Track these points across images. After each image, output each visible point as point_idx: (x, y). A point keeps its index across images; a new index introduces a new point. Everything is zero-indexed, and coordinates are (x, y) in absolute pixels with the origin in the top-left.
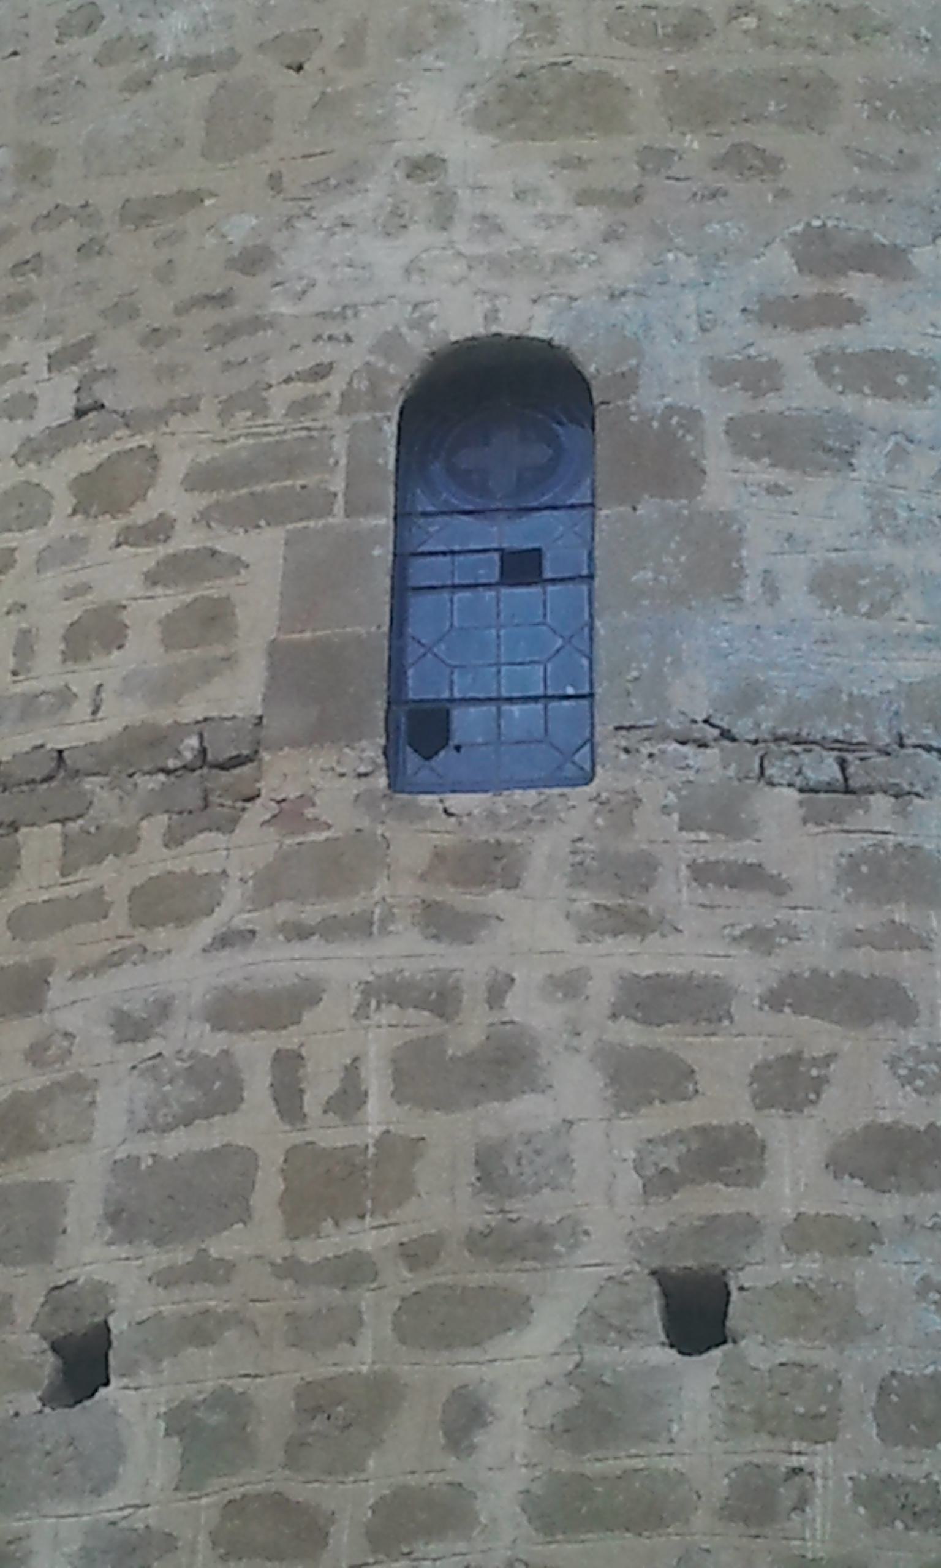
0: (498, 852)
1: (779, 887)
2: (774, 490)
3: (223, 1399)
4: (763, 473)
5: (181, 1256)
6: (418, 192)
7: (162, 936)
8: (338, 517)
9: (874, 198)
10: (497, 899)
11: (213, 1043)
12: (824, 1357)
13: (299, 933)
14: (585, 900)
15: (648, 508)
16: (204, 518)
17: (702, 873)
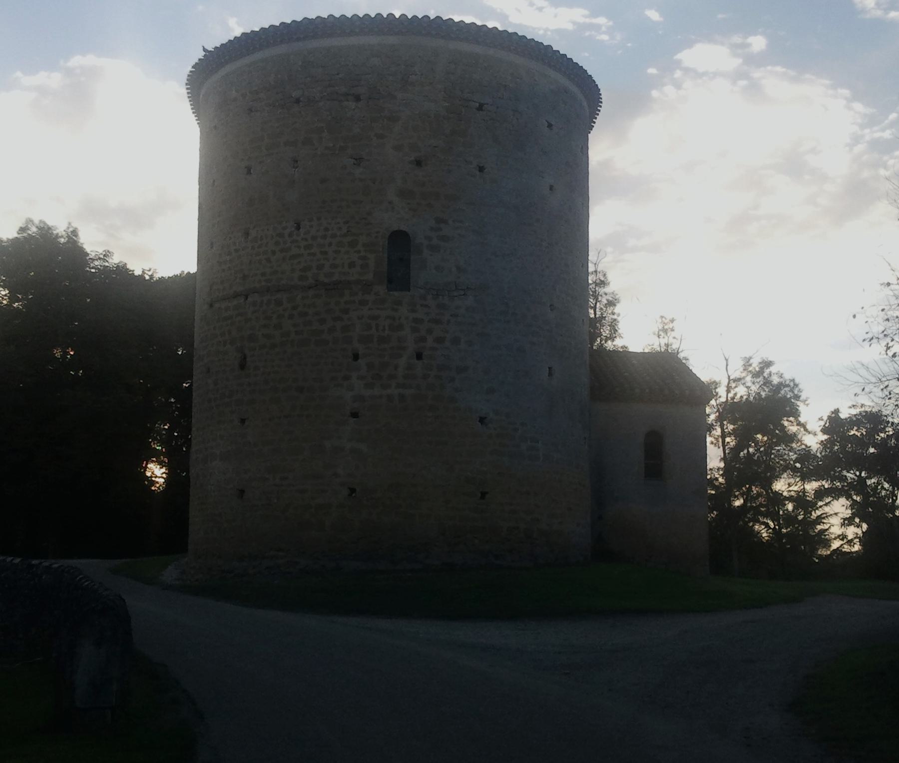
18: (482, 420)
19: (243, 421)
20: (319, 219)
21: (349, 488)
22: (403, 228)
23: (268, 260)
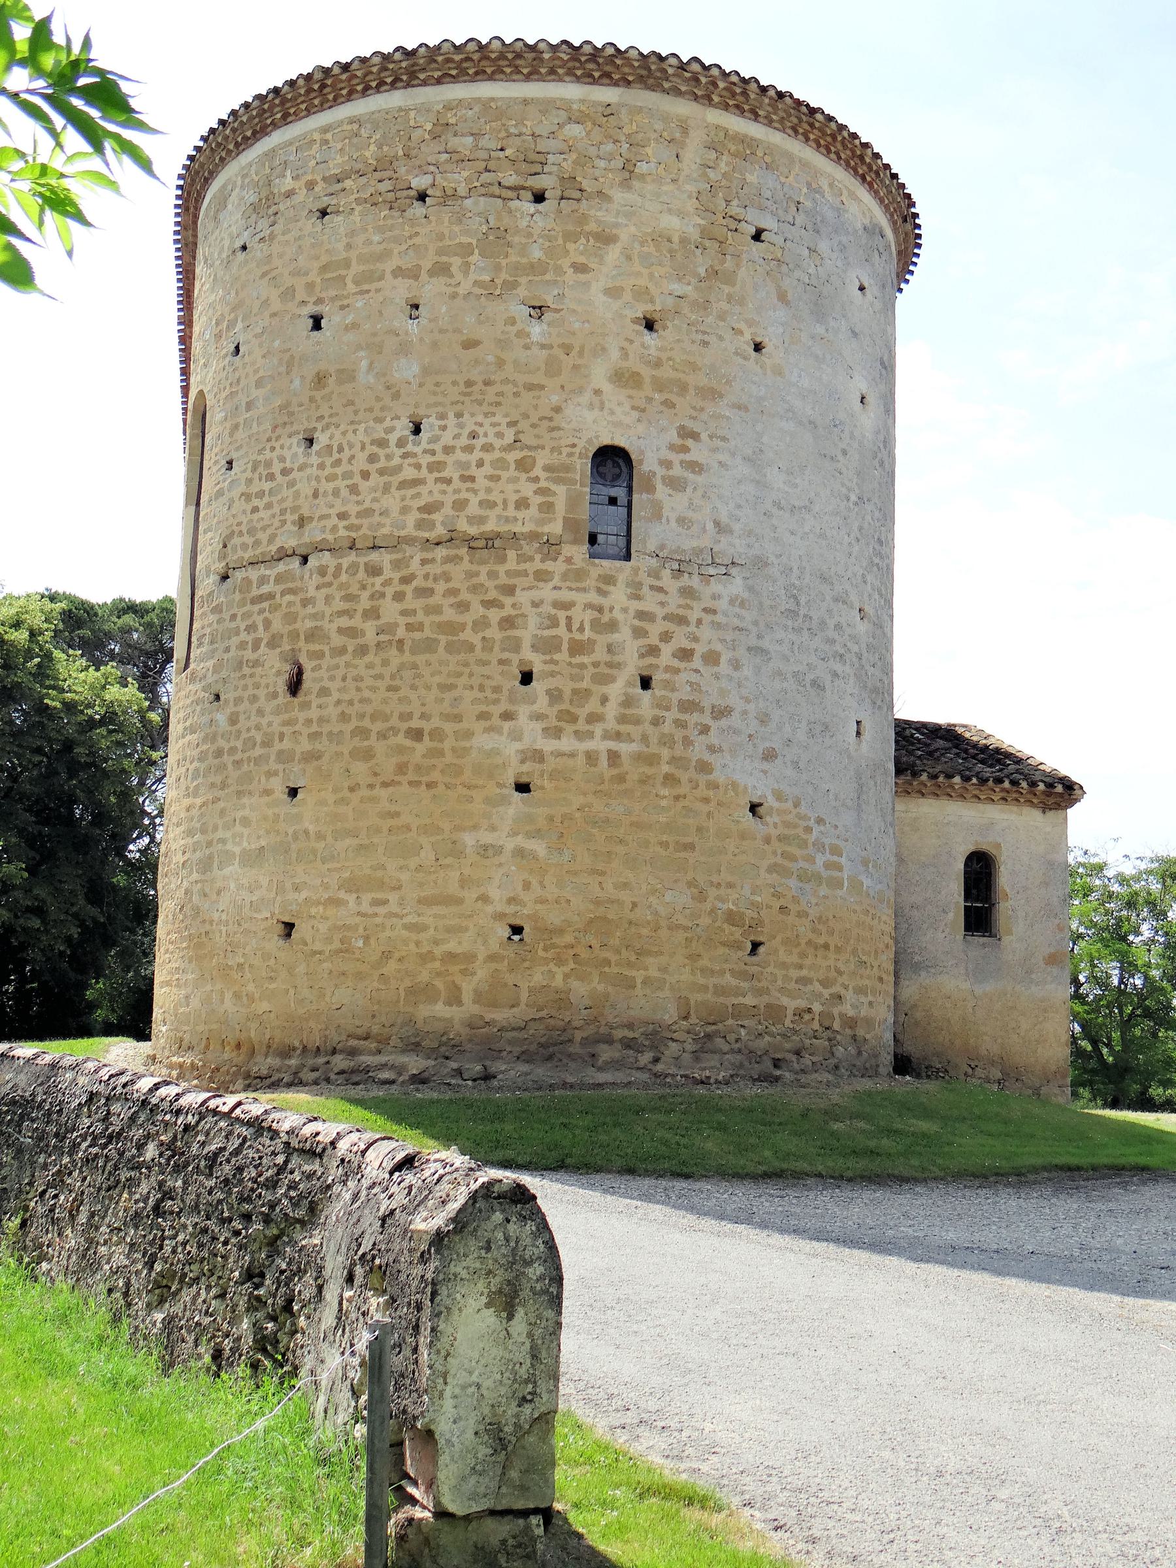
0: (612, 577)
1: (666, 593)
2: (670, 495)
3: (557, 689)
4: (668, 490)
5: (548, 657)
6: (596, 400)
7: (541, 584)
8: (578, 486)
9: (695, 418)
10: (611, 588)
11: (553, 611)
12: (670, 694)
13: (571, 589)
14: (629, 591)
15: (645, 496)
16: (547, 479)
17: (652, 587)
18: (754, 808)
19: (293, 792)
20: (459, 415)
21: (511, 926)
22: (620, 442)
23: (354, 489)
